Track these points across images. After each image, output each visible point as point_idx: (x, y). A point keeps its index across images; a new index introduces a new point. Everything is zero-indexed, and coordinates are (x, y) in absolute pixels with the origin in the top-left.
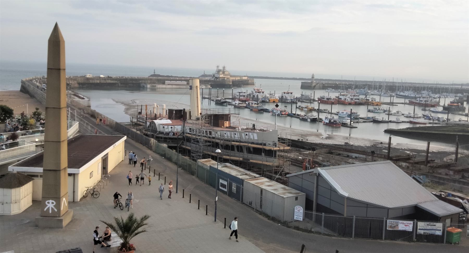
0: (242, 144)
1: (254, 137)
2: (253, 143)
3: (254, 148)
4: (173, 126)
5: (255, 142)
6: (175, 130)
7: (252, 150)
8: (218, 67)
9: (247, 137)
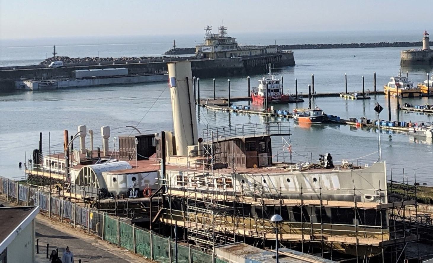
0: (306, 202)
1: (331, 185)
2: (330, 198)
3: (335, 210)
4: (136, 176)
5: (335, 195)
6: (143, 184)
7: (329, 214)
8: (208, 29)
9: (316, 185)
